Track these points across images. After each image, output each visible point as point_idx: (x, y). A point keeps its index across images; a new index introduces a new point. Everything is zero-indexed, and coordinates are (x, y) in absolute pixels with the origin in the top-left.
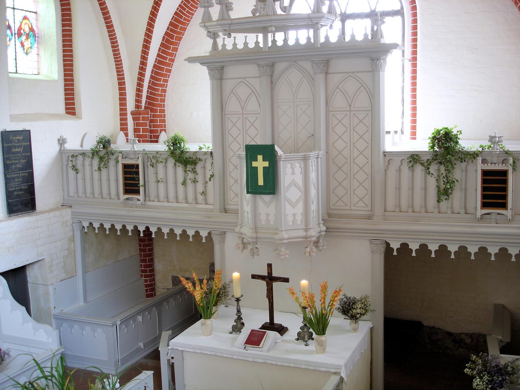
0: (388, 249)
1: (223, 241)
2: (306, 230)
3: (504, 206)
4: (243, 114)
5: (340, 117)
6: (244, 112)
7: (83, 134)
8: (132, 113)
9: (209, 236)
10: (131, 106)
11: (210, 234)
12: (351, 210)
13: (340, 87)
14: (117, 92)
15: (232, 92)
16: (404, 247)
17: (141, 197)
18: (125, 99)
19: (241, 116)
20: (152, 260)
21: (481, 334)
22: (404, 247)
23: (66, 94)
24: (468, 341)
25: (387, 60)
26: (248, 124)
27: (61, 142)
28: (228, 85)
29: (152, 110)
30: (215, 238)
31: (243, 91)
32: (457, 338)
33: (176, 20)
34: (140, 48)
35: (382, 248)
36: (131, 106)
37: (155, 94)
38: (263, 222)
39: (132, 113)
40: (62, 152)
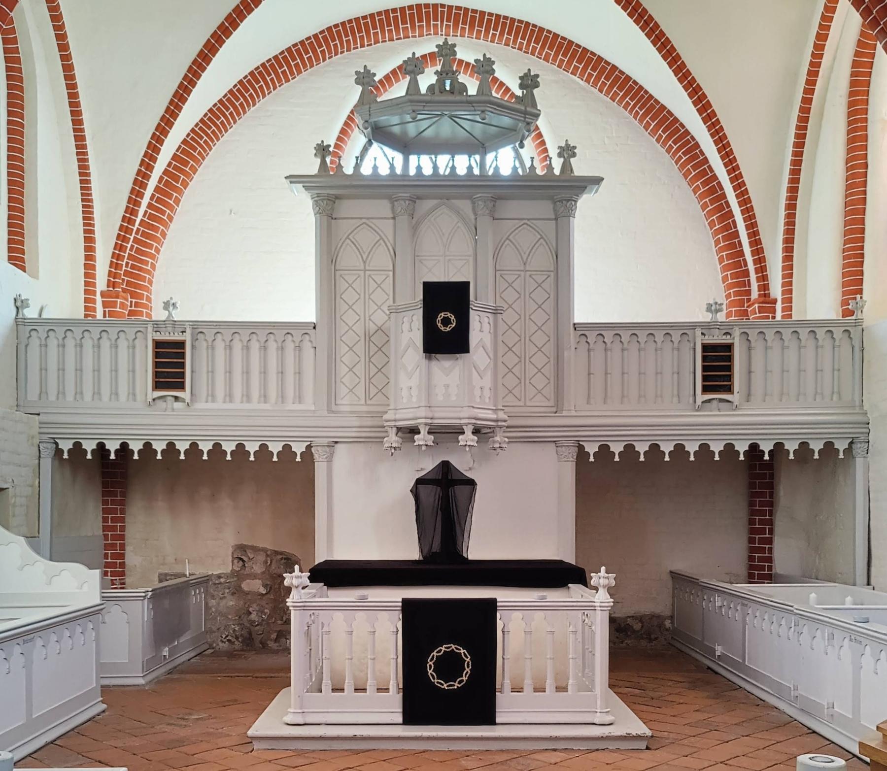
0: (582, 454)
1: (330, 460)
2: (558, 407)
3: (729, 389)
4: (365, 270)
5: (510, 279)
6: (367, 268)
7: (39, 308)
8: (103, 294)
9: (308, 454)
10: (101, 283)
11: (309, 447)
12: (525, 406)
13: (511, 237)
15: (348, 237)
16: (604, 450)
17: (185, 395)
18: (93, 267)
19: (362, 273)
21: (653, 616)
22: (604, 450)
23: (10, 233)
24: (637, 626)
25: (578, 204)
26: (373, 285)
27: (19, 304)
28: (344, 227)
29: (134, 295)
30: (318, 454)
31: (365, 238)
32: (623, 626)
33: (184, 152)
36: (101, 283)
37: (140, 269)
40: (20, 322)
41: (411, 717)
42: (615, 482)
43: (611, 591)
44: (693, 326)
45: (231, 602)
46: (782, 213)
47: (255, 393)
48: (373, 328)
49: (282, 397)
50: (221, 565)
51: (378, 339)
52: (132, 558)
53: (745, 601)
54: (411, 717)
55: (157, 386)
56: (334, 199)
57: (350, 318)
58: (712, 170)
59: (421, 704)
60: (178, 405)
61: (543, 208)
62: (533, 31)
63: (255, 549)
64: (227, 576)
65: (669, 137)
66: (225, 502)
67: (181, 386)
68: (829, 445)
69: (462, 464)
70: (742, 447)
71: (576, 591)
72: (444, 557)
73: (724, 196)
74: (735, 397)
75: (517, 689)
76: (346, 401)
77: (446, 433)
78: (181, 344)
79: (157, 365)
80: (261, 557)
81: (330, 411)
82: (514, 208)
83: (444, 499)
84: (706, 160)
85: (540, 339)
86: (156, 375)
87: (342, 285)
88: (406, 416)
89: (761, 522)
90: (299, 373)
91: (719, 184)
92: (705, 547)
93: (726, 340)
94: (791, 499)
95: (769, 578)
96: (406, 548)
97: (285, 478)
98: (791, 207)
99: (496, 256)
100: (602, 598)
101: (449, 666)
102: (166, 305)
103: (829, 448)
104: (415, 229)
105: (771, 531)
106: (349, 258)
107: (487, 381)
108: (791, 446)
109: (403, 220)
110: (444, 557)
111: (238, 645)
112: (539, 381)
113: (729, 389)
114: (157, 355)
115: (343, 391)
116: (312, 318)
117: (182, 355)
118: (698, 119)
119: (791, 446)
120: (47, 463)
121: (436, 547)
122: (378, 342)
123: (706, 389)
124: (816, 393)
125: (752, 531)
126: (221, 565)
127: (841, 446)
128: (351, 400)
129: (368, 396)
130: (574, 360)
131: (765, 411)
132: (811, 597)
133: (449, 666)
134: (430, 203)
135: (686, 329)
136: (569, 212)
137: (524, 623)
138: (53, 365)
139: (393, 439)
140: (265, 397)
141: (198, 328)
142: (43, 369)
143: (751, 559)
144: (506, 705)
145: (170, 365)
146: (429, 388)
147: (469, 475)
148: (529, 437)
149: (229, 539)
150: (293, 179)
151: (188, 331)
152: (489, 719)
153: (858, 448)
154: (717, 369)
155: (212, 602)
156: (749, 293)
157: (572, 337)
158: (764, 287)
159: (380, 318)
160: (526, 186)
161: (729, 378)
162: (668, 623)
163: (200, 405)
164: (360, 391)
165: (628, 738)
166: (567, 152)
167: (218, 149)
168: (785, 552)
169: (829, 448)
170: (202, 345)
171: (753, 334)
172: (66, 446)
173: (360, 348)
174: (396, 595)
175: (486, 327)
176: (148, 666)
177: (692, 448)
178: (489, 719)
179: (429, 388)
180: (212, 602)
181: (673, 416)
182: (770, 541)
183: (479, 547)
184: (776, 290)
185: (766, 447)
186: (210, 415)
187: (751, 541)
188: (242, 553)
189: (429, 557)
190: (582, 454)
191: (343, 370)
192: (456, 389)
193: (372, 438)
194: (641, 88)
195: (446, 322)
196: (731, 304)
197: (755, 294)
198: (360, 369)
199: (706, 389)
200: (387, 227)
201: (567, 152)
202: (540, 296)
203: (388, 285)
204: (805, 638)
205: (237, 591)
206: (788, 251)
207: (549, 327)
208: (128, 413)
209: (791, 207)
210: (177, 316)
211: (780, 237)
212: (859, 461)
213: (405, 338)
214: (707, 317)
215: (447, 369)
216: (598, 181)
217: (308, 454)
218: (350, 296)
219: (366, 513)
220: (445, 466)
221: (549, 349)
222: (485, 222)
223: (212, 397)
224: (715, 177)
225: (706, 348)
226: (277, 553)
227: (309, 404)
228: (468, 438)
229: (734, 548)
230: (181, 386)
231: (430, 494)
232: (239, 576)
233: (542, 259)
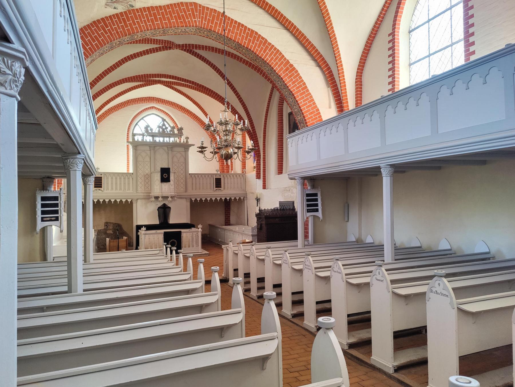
0: (191, 200)
3: (221, 187)
9: (131, 202)
16: (196, 200)
22: (196, 200)
35: (190, 200)
42: (197, 206)
43: (201, 228)
44: (213, 174)
47: (118, 188)
51: (147, 176)
53: (225, 229)
55: (95, 187)
56: (136, 146)
57: (140, 172)
60: (100, 191)
61: (182, 149)
66: (102, 212)
67: (101, 187)
68: (240, 198)
70: (223, 199)
71: (193, 229)
74: (222, 189)
76: (139, 190)
77: (165, 198)
78: (101, 178)
80: (112, 225)
82: (176, 149)
83: (164, 211)
85: (182, 181)
87: (138, 165)
88: (156, 194)
92: (216, 218)
93: (220, 177)
94: (234, 209)
95: (230, 225)
96: (156, 221)
97: (126, 208)
99: (172, 158)
100: (200, 230)
104: (155, 153)
106: (140, 159)
107: (173, 187)
108: (233, 198)
109: (152, 151)
112: (182, 185)
113: (221, 187)
115: (139, 188)
117: (101, 180)
119: (233, 198)
122: (148, 178)
123: (216, 187)
125: (226, 215)
127: (242, 198)
128: (141, 190)
129: (145, 189)
130: (189, 181)
131: (228, 192)
132: (237, 228)
134: (158, 147)
136: (188, 151)
138: (118, 183)
139: (153, 199)
140: (121, 189)
145: (98, 183)
146: (162, 189)
147: (169, 206)
148: (180, 197)
149: (104, 221)
153: (245, 198)
154: (218, 183)
157: (189, 176)
160: (180, 145)
163: (105, 191)
164: (143, 188)
165: (205, 254)
166: (187, 138)
168: (233, 219)
171: (225, 176)
173: (143, 178)
174: (163, 231)
177: (214, 199)
179: (162, 189)
181: (209, 192)
183: (172, 221)
185: (228, 199)
187: (226, 217)
188: (107, 224)
190: (191, 200)
191: (139, 183)
192: (167, 189)
193: (148, 198)
195: (165, 175)
196: (220, 170)
197: (225, 164)
198: (143, 183)
199: (216, 187)
200: (149, 152)
201: (187, 138)
202: (182, 167)
203: (149, 165)
204: (237, 236)
213: (156, 178)
214: (216, 172)
215: (165, 185)
216: (194, 145)
217: (131, 202)
218: (140, 167)
220: (164, 204)
221: (184, 179)
222: (170, 152)
223: (108, 189)
227: (131, 191)
228: (170, 199)
230: (101, 187)
231: (162, 210)
233: (182, 160)
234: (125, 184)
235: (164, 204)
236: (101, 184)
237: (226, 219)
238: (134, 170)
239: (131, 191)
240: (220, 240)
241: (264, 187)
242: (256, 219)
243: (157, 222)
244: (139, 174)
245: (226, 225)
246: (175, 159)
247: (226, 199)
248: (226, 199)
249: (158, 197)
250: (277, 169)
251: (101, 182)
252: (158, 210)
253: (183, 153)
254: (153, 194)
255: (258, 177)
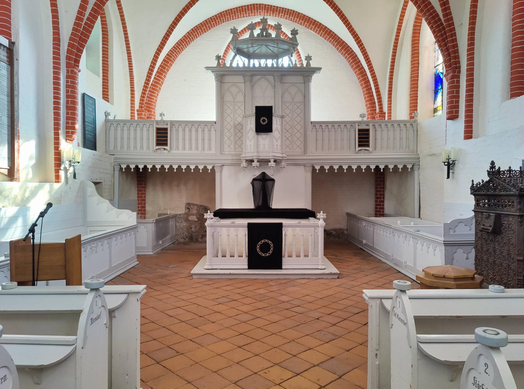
0: (314, 169)
1: (221, 172)
3: (368, 146)
8: (137, 111)
9: (213, 170)
11: (213, 167)
14: (130, 96)
17: (167, 148)
20: (145, 204)
22: (322, 168)
23: (103, 88)
24: (334, 233)
26: (237, 107)
29: (149, 111)
30: (217, 170)
31: (234, 90)
33: (167, 58)
34: (147, 70)
37: (151, 101)
38: (262, 149)
39: (137, 111)
41: (251, 266)
42: (326, 180)
43: (325, 220)
44: (355, 122)
45: (185, 224)
46: (388, 81)
47: (187, 146)
48: (237, 123)
49: (203, 149)
50: (181, 211)
52: (148, 208)
53: (374, 223)
54: (251, 266)
55: (158, 144)
57: (229, 119)
58: (362, 65)
59: (255, 262)
60: (165, 151)
62: (296, 14)
63: (193, 204)
64: (183, 214)
65: (346, 53)
66: (183, 187)
67: (166, 144)
69: (270, 173)
70: (373, 167)
71: (312, 220)
72: (263, 207)
73: (366, 75)
75: (290, 256)
76: (227, 150)
77: (264, 162)
79: (157, 137)
80: (196, 208)
81: (221, 153)
83: (263, 186)
84: (360, 61)
86: (157, 140)
87: (226, 107)
89: (380, 195)
90: (210, 140)
91: (364, 70)
92: (360, 204)
94: (391, 186)
95: (383, 215)
96: (248, 203)
98: (391, 78)
100: (321, 223)
101: (265, 248)
102: (161, 115)
103: (405, 167)
104: (252, 87)
105: (384, 198)
106: (228, 97)
107: (279, 143)
108: (391, 167)
109: (248, 84)
110: (263, 207)
111: (187, 240)
113: (368, 146)
114: (157, 133)
116: (214, 119)
117: (167, 133)
118: (357, 46)
119: (391, 167)
120: (117, 173)
121: (260, 204)
122: (239, 129)
124: (400, 147)
126: (181, 211)
127: (409, 166)
129: (235, 149)
131: (382, 153)
132: (398, 222)
133: (265, 248)
134: (258, 77)
135: (352, 123)
136: (309, 81)
137: (292, 232)
139: (244, 164)
140: (197, 149)
141: (172, 123)
142: (116, 138)
143: (376, 208)
144: (286, 262)
145: (162, 137)
146: (258, 146)
147: (272, 177)
148: (294, 163)
149: (184, 201)
150: (207, 68)
151: (169, 124)
152: (280, 267)
153: (416, 167)
154: (364, 138)
155: (178, 224)
156: (375, 110)
157: (310, 126)
158: (381, 108)
159: (239, 119)
160: (293, 71)
161: (368, 141)
162: (345, 232)
163: (173, 152)
164: (232, 146)
165: (331, 274)
167: (180, 57)
168: (389, 206)
169: (405, 167)
170: (174, 129)
171: (377, 126)
172: (124, 166)
173: (232, 131)
174: (245, 222)
175: (279, 123)
176: (154, 247)
178: (280, 267)
179: (258, 146)
180: (178, 224)
181: (346, 155)
182: (383, 202)
183: (276, 204)
184: (385, 109)
185: (382, 167)
186: (178, 154)
187: (376, 201)
188: (189, 206)
189: (257, 208)
190: (314, 169)
191: (226, 138)
192: (268, 146)
193: (236, 164)
194: (336, 35)
195: (264, 120)
197: (378, 110)
198: (232, 138)
200: (242, 86)
203: (242, 107)
204: (396, 237)
205: (187, 220)
206: (390, 97)
207: (302, 123)
208: (146, 154)
209: (391, 78)
210: (165, 118)
211: (387, 90)
212: (416, 172)
213: (249, 127)
214: (360, 119)
215: (264, 138)
216: (320, 69)
217: (213, 170)
218: (228, 111)
219: (234, 191)
220: (264, 174)
221: (302, 131)
222: (278, 84)
223: (178, 148)
224: (363, 68)
225: (360, 130)
226: (201, 206)
227: (213, 151)
228: (272, 164)
229: (370, 204)
230: (166, 144)
231: (258, 184)
232: (187, 214)
233: (299, 98)
234: (197, 139)
235: (264, 174)
236: (167, 140)
237: (377, 205)
238: (217, 117)
239: (213, 151)
240: (364, 242)
241: (469, 134)
242: (471, 201)
243: (250, 205)
244: (226, 123)
245: (376, 215)
246: (287, 98)
247: (377, 167)
248: (377, 167)
249: (252, 161)
250: (508, 88)
251: (167, 137)
252: (252, 183)
253: (302, 86)
254: (243, 155)
255: (452, 115)
